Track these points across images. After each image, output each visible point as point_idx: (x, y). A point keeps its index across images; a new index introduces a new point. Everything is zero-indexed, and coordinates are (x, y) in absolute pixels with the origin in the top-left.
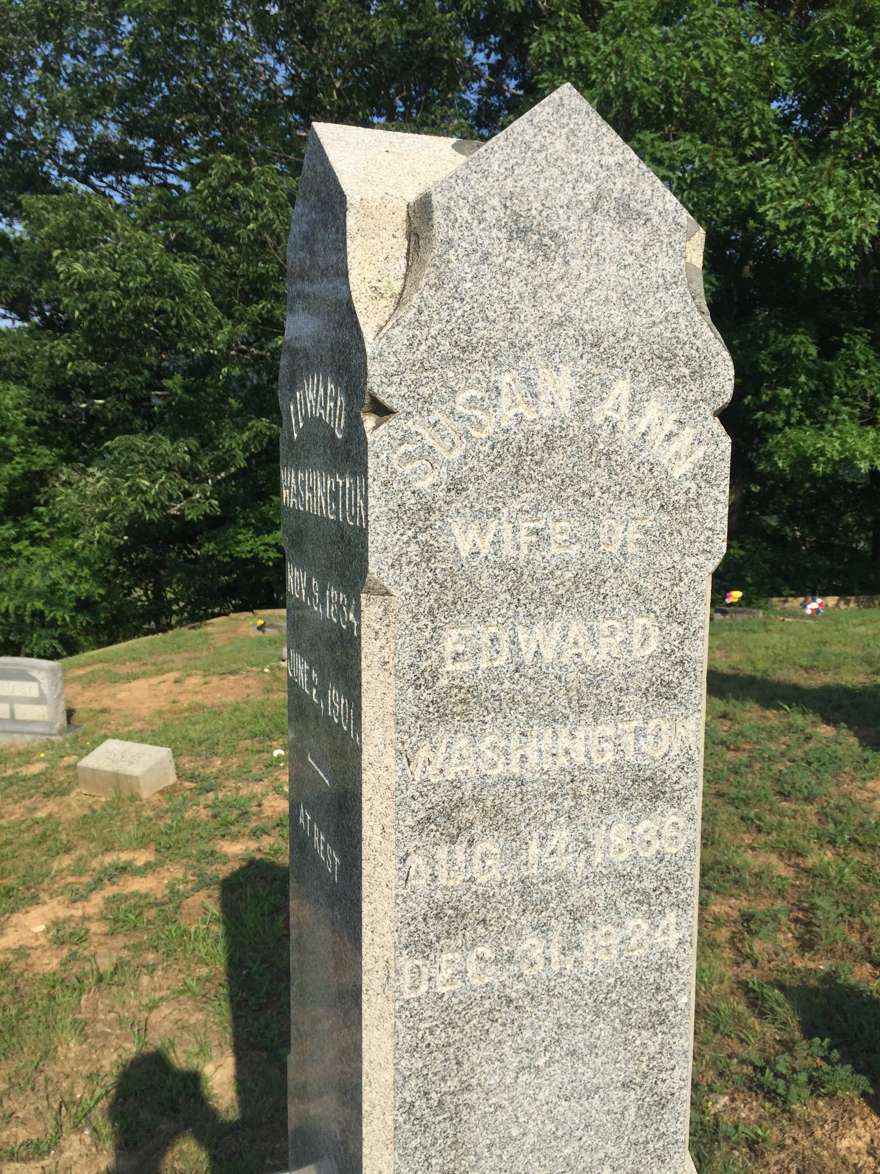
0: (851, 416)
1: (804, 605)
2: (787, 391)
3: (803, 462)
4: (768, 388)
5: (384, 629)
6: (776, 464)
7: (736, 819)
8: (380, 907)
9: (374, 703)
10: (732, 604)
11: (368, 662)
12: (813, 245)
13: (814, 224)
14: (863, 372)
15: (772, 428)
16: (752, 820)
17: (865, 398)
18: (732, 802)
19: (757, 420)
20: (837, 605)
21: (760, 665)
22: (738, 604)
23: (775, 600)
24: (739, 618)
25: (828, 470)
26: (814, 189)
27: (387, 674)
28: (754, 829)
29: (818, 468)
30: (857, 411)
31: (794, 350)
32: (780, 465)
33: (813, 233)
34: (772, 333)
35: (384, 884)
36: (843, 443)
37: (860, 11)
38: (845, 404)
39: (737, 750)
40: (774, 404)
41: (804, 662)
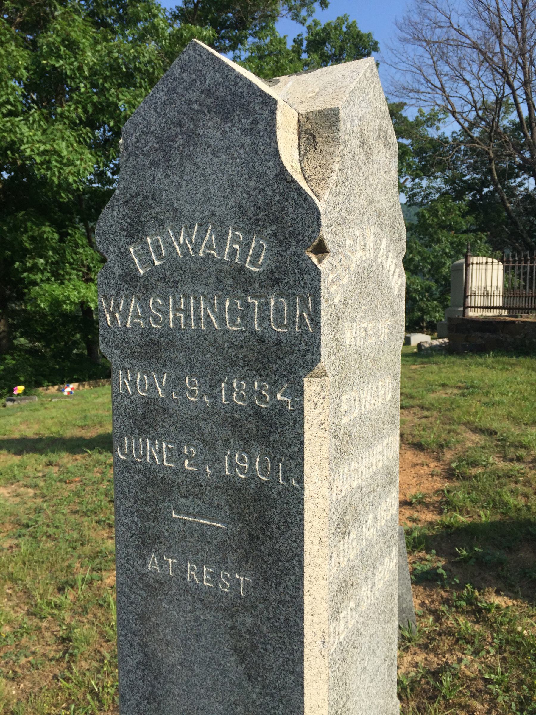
0: (78, 275)
1: (61, 390)
2: (42, 261)
3: (56, 303)
4: (30, 258)
5: (321, 401)
6: (39, 305)
7: (94, 524)
8: (318, 596)
9: (314, 453)
10: (18, 395)
11: (309, 425)
12: (57, 173)
13: (57, 161)
14: (81, 251)
15: (35, 283)
16: (104, 521)
17: (84, 266)
18: (85, 514)
19: (24, 278)
20: (78, 389)
21: (54, 429)
22: (25, 393)
23: (40, 389)
24: (24, 403)
25: (73, 309)
26: (54, 140)
27: (323, 431)
28: (107, 527)
29: (67, 307)
30: (80, 273)
31: (45, 236)
32: (42, 306)
33: (56, 166)
34: (29, 224)
35: (321, 579)
36: (79, 293)
37: (68, 40)
38: (73, 269)
39: (71, 482)
40: (34, 268)
41: (79, 423)
